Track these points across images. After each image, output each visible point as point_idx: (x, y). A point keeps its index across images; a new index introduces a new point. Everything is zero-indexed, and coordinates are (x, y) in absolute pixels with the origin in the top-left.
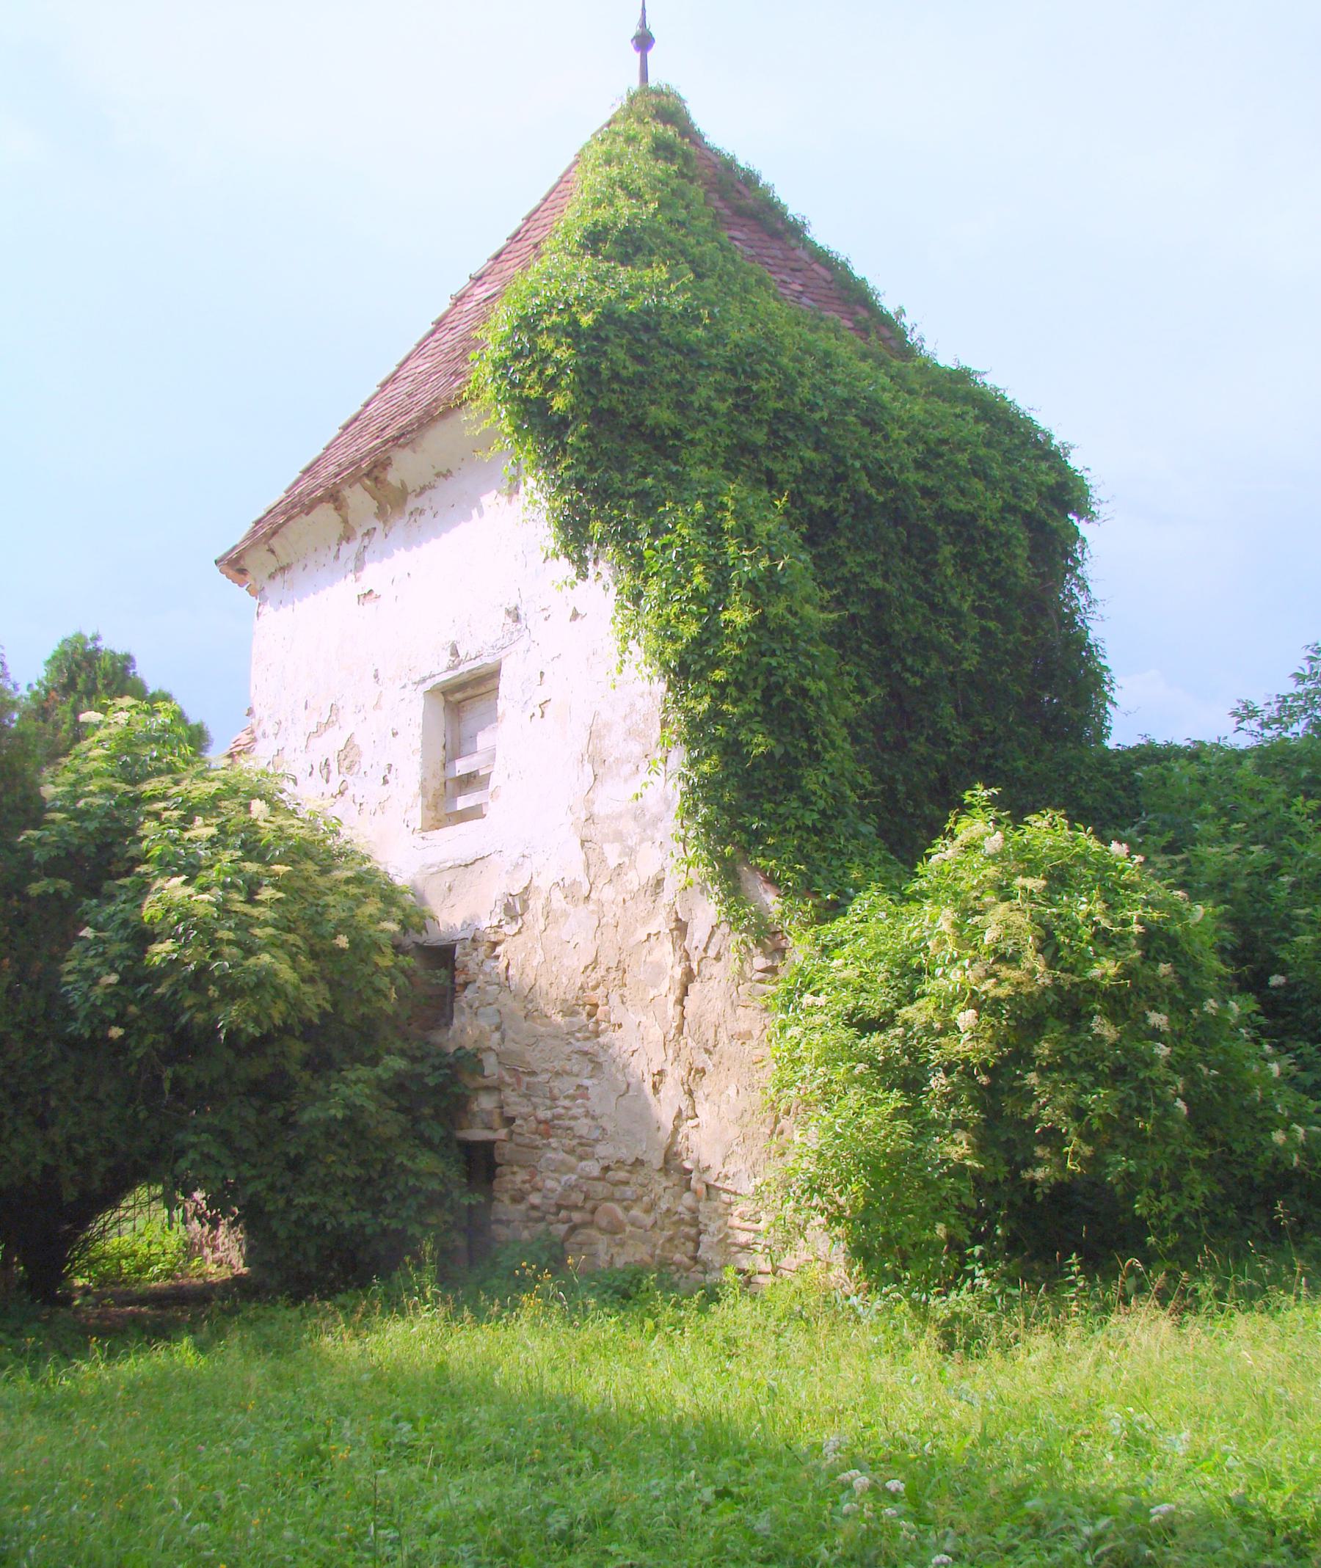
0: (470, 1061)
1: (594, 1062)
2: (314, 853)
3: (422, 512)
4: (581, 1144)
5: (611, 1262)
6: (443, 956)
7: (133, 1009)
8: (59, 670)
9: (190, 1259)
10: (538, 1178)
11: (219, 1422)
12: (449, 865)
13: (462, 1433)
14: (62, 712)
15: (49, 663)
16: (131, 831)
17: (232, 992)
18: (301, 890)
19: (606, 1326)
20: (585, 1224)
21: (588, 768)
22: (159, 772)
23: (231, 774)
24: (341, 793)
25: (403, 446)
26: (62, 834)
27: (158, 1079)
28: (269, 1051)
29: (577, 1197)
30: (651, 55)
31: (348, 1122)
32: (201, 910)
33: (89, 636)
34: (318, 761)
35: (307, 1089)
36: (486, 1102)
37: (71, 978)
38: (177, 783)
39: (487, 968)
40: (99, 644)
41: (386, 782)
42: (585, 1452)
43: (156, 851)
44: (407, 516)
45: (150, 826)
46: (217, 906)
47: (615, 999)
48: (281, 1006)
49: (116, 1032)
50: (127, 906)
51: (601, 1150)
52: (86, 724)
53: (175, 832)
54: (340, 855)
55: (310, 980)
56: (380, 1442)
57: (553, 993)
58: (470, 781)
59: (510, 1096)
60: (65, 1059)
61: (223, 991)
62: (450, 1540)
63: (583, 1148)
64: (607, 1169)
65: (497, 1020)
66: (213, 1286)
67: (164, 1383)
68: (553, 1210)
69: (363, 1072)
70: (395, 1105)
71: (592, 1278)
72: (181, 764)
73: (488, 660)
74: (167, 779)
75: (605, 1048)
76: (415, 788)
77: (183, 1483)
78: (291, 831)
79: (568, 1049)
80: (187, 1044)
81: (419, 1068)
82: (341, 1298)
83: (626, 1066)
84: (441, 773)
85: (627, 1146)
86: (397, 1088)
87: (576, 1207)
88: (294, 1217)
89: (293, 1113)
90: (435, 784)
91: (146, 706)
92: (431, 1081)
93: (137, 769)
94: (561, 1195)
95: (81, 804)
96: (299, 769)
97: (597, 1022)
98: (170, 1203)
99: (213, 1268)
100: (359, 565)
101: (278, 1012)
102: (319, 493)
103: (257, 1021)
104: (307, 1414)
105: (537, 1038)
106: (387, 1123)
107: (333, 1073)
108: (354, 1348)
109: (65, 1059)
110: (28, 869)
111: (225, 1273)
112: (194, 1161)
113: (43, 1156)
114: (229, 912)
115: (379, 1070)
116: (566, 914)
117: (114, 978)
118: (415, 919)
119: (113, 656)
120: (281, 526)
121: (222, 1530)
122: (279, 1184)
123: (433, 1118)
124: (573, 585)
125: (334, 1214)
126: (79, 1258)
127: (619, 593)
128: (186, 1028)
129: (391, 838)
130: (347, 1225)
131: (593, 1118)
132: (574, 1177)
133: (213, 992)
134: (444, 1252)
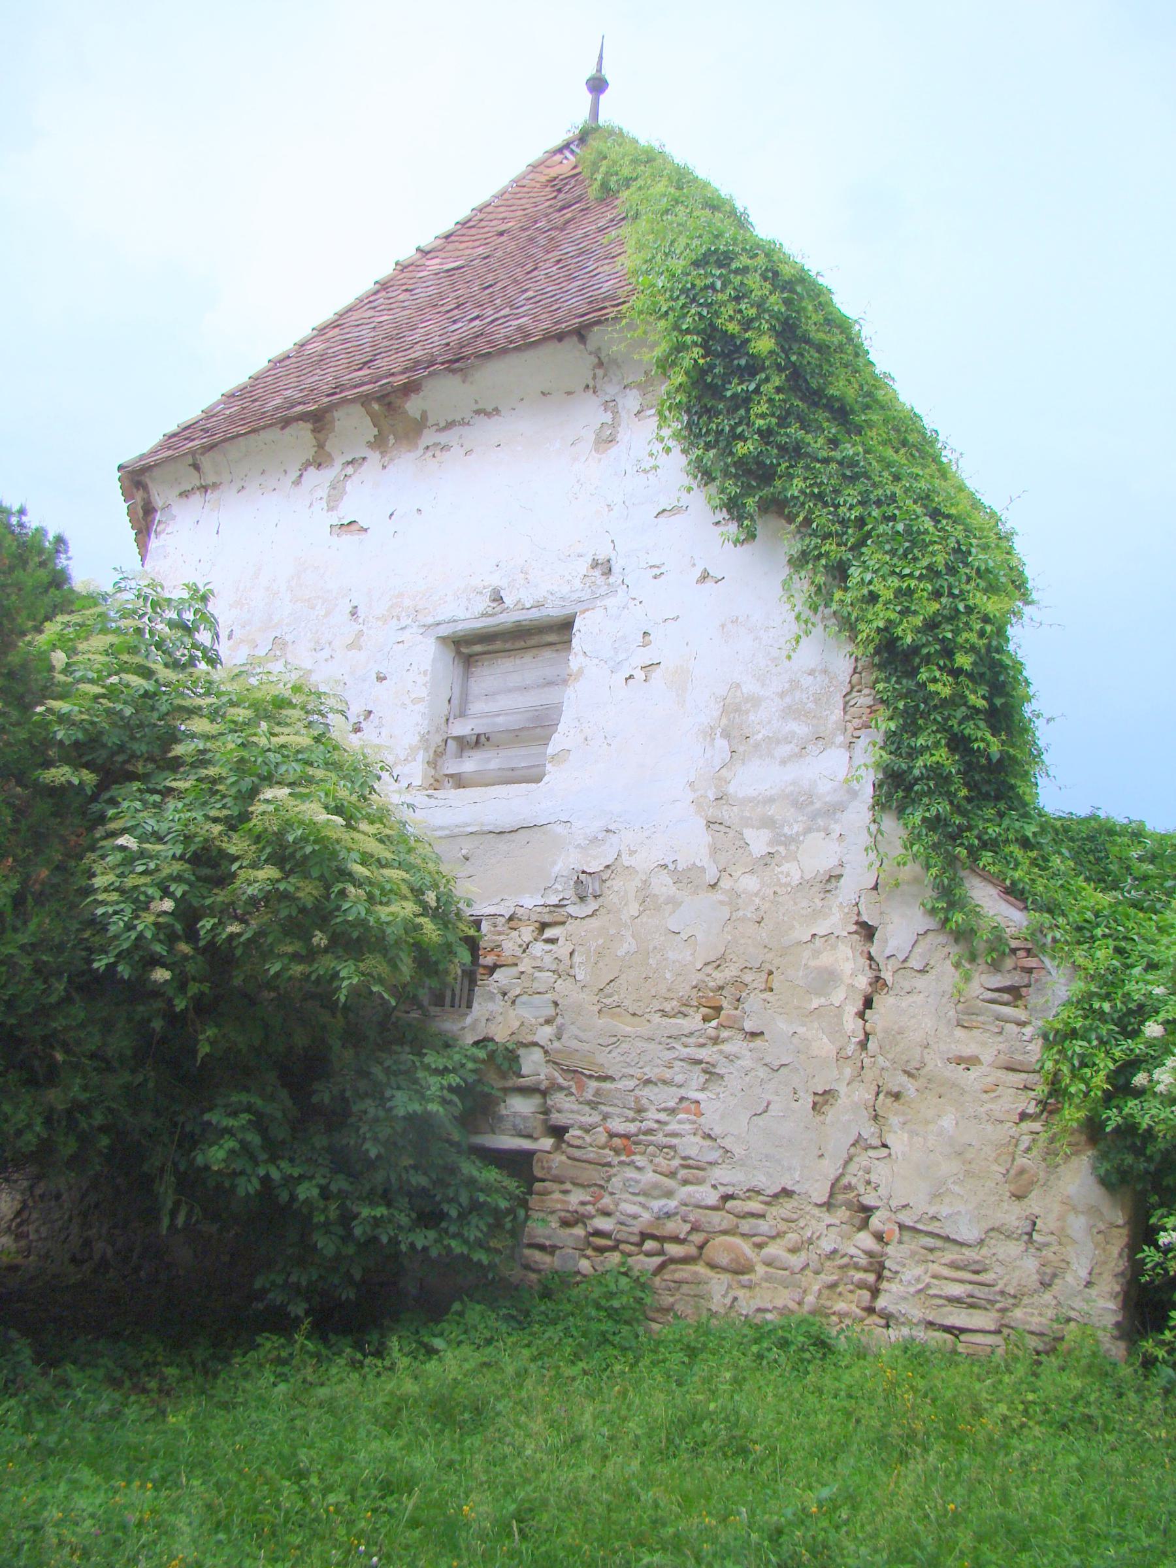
0: (503, 1059)
3: (445, 448)
12: (470, 829)
25: (454, 371)
29: (673, 1226)
30: (603, 98)
36: (521, 1107)
40: (24, 519)
44: (421, 451)
51: (720, 1174)
64: (726, 1198)
65: (551, 1011)
68: (636, 1239)
73: (568, 611)
79: (671, 1055)
87: (676, 1239)
94: (651, 1224)
117: (168, 905)
133: (320, 939)
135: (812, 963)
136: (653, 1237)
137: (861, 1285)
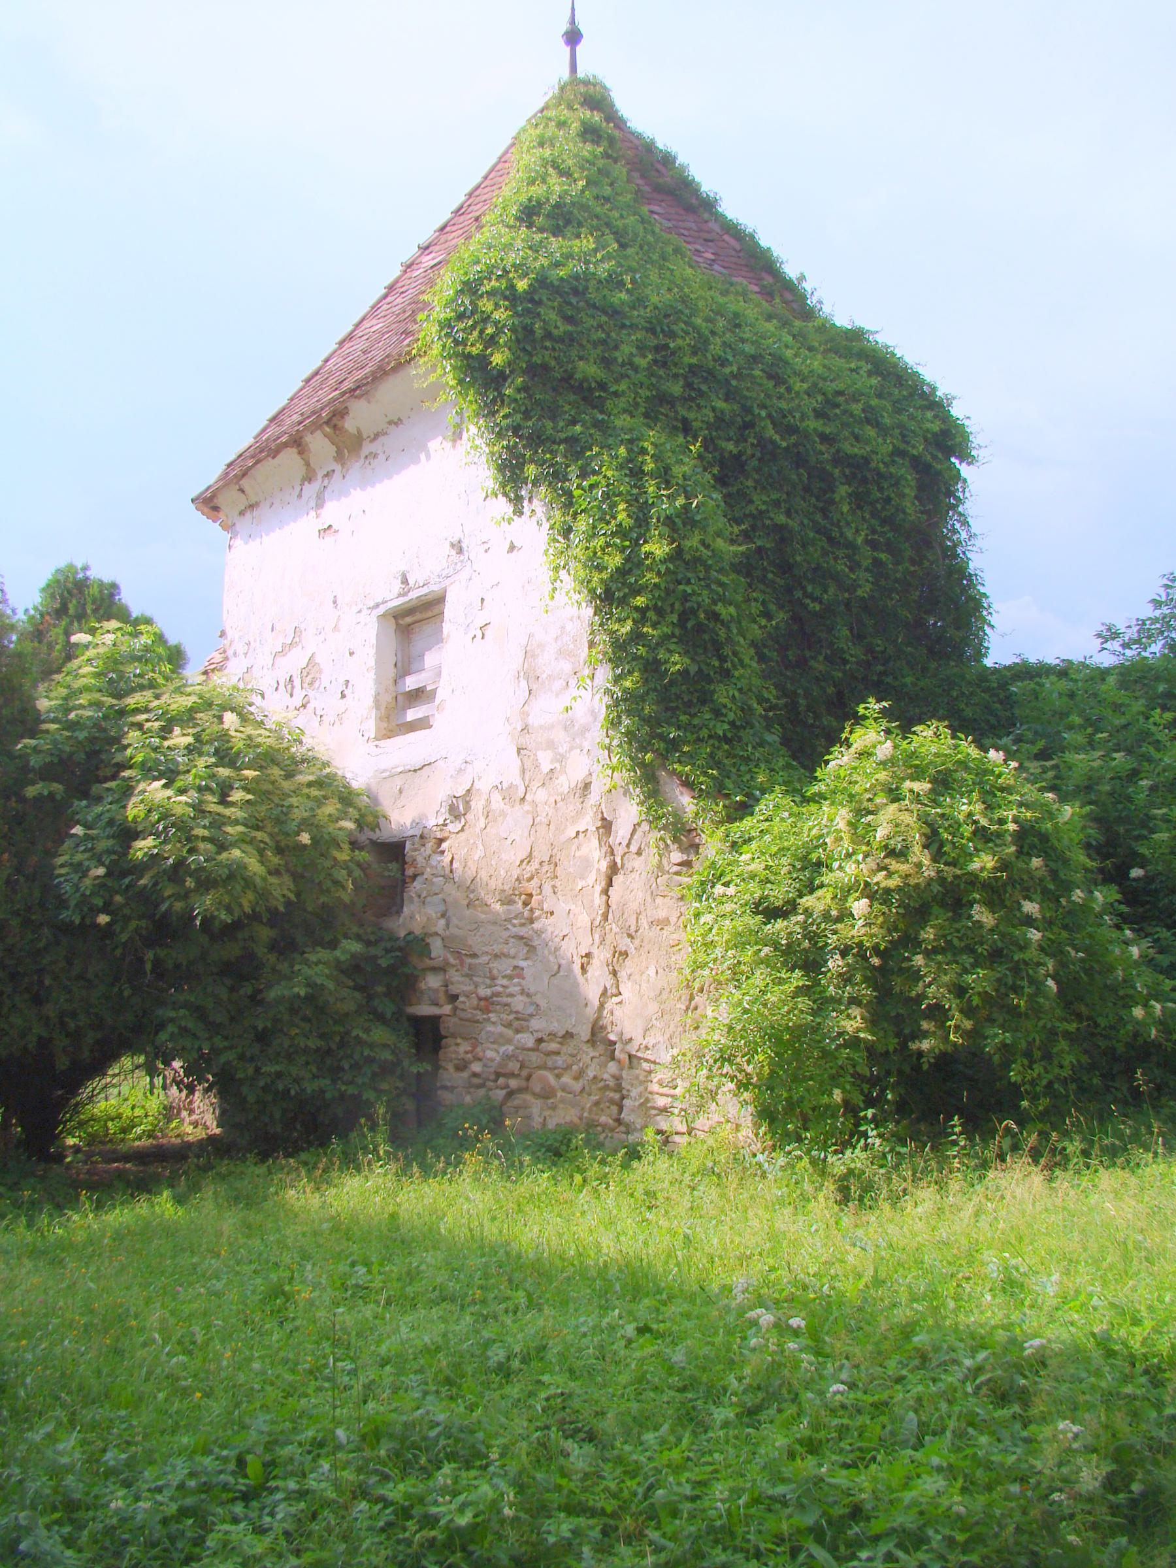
0: (418, 944)
1: (529, 945)
2: (280, 759)
3: (375, 456)
4: (517, 1019)
5: (544, 1124)
6: (394, 851)
7: (118, 899)
8: (53, 596)
9: (169, 1121)
11: (195, 1267)
13: (412, 1276)
14: (56, 633)
15: (43, 590)
16: (117, 740)
17: (206, 883)
18: (268, 792)
19: (539, 1180)
20: (520, 1090)
21: (524, 684)
22: (142, 688)
23: (206, 689)
24: (304, 706)
26: (55, 742)
27: (141, 961)
29: (514, 1066)
30: (579, 49)
31: (310, 999)
32: (178, 810)
33: (80, 566)
35: (274, 970)
36: (433, 981)
39: (433, 862)
40: (88, 573)
41: (343, 696)
43: (139, 758)
45: (133, 736)
47: (547, 889)
48: (250, 895)
49: (103, 919)
50: (113, 807)
51: (535, 1024)
52: (77, 645)
53: (156, 741)
54: (303, 761)
55: (275, 872)
56: (338, 1284)
57: (493, 884)
58: (418, 696)
59: (455, 976)
63: (519, 1022)
64: (540, 1041)
65: (442, 908)
66: (189, 1145)
67: (146, 1231)
68: (492, 1077)
69: (323, 954)
70: (352, 984)
71: (527, 1138)
72: (161, 681)
73: (434, 588)
74: (149, 694)
75: (539, 933)
76: (370, 701)
77: (163, 1320)
78: (259, 740)
79: (506, 934)
80: (166, 929)
81: (373, 951)
82: (304, 1156)
83: (557, 949)
84: (392, 688)
86: (353, 969)
87: (512, 1075)
88: (262, 1083)
89: (261, 991)
90: (387, 698)
91: (130, 629)
92: (384, 963)
93: (122, 684)
95: (72, 716)
96: (266, 684)
97: (532, 910)
98: (152, 1071)
99: (190, 1129)
100: (320, 503)
101: (247, 901)
102: (284, 439)
103: (229, 909)
104: (273, 1259)
105: (478, 925)
106: (345, 1000)
107: (296, 956)
108: (315, 1201)
110: (25, 774)
111: (200, 1134)
112: (172, 1034)
113: (38, 1030)
114: (204, 812)
115: (338, 953)
116: (503, 814)
117: (101, 871)
118: (369, 818)
119: (101, 584)
120: (250, 468)
122: (248, 1054)
123: (385, 995)
124: (510, 521)
125: (297, 1081)
126: (70, 1120)
127: (551, 528)
128: (165, 915)
129: (348, 746)
131: (528, 995)
132: (511, 1048)
133: (190, 883)
135: (578, 854)
137: (612, 1102)
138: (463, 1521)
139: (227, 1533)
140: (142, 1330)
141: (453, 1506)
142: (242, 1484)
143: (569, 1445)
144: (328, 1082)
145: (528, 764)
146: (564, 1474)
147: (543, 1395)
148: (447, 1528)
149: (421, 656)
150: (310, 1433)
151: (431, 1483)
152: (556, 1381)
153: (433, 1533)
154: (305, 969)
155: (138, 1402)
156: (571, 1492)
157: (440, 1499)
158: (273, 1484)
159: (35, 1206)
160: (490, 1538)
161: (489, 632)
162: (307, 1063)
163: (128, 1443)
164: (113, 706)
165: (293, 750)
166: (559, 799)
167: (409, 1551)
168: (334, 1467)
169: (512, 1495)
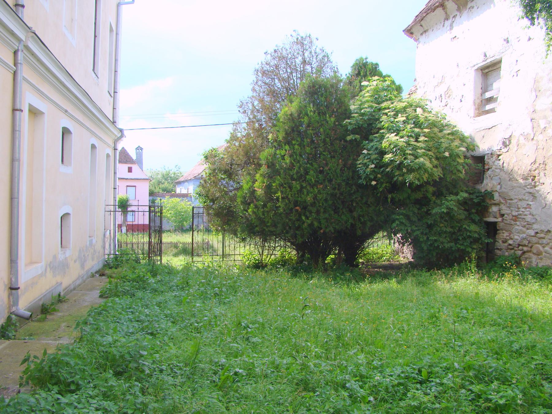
0: (489, 195)
1: (533, 196)
2: (437, 126)
3: (473, 7)
4: (528, 224)
5: (537, 265)
6: (480, 159)
7: (379, 176)
8: (355, 69)
9: (395, 256)
10: (512, 235)
11: (404, 305)
13: (483, 315)
14: (356, 82)
15: (352, 67)
16: (378, 119)
17: (411, 170)
18: (433, 137)
19: (534, 285)
20: (528, 252)
21: (534, 94)
22: (387, 100)
23: (410, 100)
24: (446, 105)
26: (357, 121)
27: (387, 198)
28: (422, 190)
29: (526, 242)
31: (448, 213)
32: (401, 144)
33: (364, 58)
34: (438, 95)
35: (434, 202)
36: (494, 209)
37: (360, 166)
38: (392, 103)
39: (496, 164)
41: (461, 101)
42: (526, 326)
43: (386, 125)
45: (384, 117)
46: (406, 143)
47: (542, 174)
48: (426, 175)
49: (374, 183)
50: (377, 143)
51: (535, 226)
52: (363, 86)
53: (392, 119)
54: (446, 126)
55: (436, 167)
56: (456, 315)
57: (519, 172)
58: (490, 100)
59: (503, 207)
60: (358, 191)
61: (408, 170)
62: (479, 348)
63: (529, 226)
64: (537, 233)
65: (499, 181)
66: (402, 265)
67: (389, 292)
69: (453, 197)
70: (463, 208)
71: (530, 269)
72: (393, 98)
73: (497, 57)
74: (389, 102)
75: (538, 191)
76: (471, 103)
77: (393, 321)
78: (430, 118)
79: (525, 191)
80: (395, 187)
81: (472, 196)
82: (443, 270)
83: (545, 198)
84: (480, 97)
85: (545, 226)
86: (464, 203)
87: (525, 246)
88: (429, 243)
89: (430, 210)
90: (478, 101)
91: (382, 79)
92: (476, 201)
93: (380, 100)
95: (362, 111)
96: (432, 98)
97: (535, 182)
98: (390, 238)
99: (402, 259)
100: (451, 29)
101: (425, 177)
102: (437, 4)
103: (418, 180)
104: (432, 305)
105: (513, 188)
106: (461, 214)
107: (443, 198)
108: (448, 286)
109: (358, 191)
110: (347, 132)
111: (406, 261)
112: (397, 224)
113: (351, 221)
114: (409, 144)
115: (459, 197)
116: (524, 145)
117: (373, 166)
118: (471, 146)
119: (372, 64)
120: (425, 17)
121: (405, 335)
122: (424, 232)
123: (476, 213)
124: (529, 28)
125: (442, 243)
126: (361, 253)
127: (547, 29)
128: (395, 181)
129: (463, 120)
130: (446, 247)
131: (533, 215)
132: (525, 235)
133: (404, 170)
134: (479, 258)
136: (522, 245)
138: (502, 402)
139: (414, 393)
140: (386, 323)
141: (497, 397)
142: (420, 378)
143: (544, 382)
144: (453, 244)
145: (535, 125)
146: (541, 392)
147: (534, 363)
148: (495, 403)
149: (492, 84)
150: (445, 364)
151: (489, 387)
152: (539, 358)
153: (490, 404)
154: (446, 202)
155: (383, 347)
156: (545, 400)
157: (492, 393)
158: (431, 379)
159: (349, 281)
160: (511, 410)
161: (519, 73)
162: (446, 237)
163: (381, 359)
164: (376, 107)
165: (442, 122)
166: (548, 139)
167: (480, 410)
168: (453, 376)
169: (521, 396)
